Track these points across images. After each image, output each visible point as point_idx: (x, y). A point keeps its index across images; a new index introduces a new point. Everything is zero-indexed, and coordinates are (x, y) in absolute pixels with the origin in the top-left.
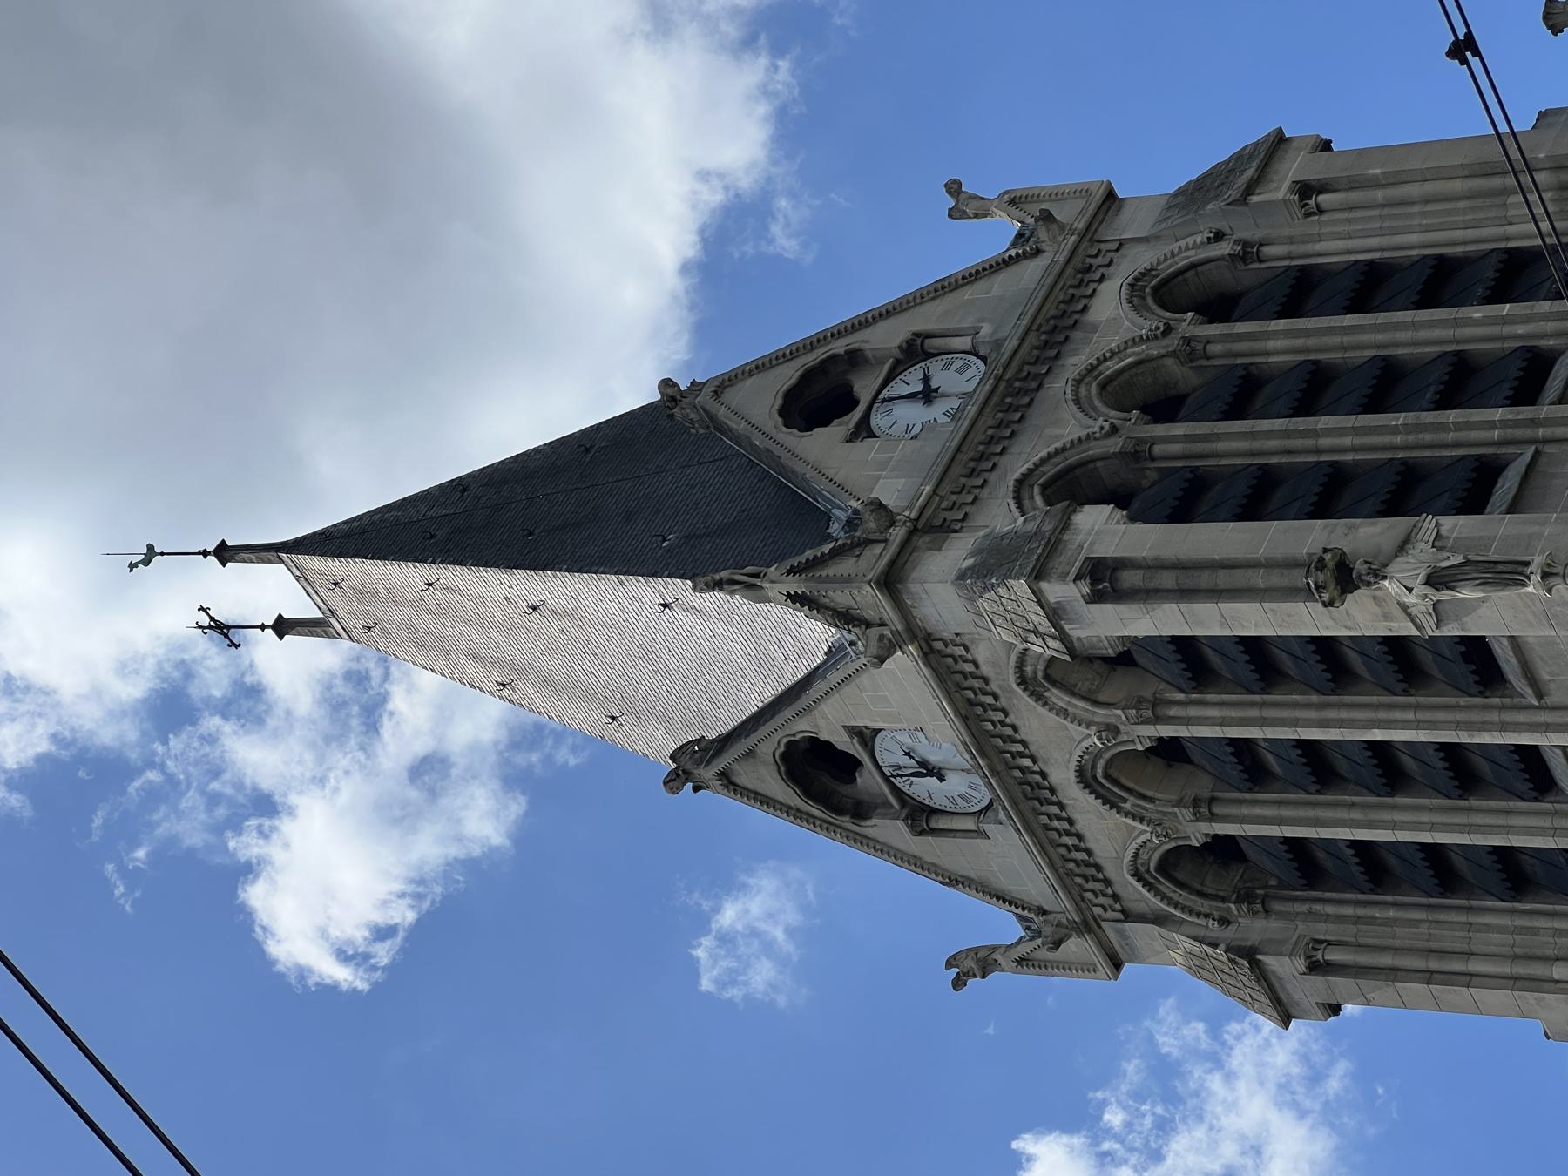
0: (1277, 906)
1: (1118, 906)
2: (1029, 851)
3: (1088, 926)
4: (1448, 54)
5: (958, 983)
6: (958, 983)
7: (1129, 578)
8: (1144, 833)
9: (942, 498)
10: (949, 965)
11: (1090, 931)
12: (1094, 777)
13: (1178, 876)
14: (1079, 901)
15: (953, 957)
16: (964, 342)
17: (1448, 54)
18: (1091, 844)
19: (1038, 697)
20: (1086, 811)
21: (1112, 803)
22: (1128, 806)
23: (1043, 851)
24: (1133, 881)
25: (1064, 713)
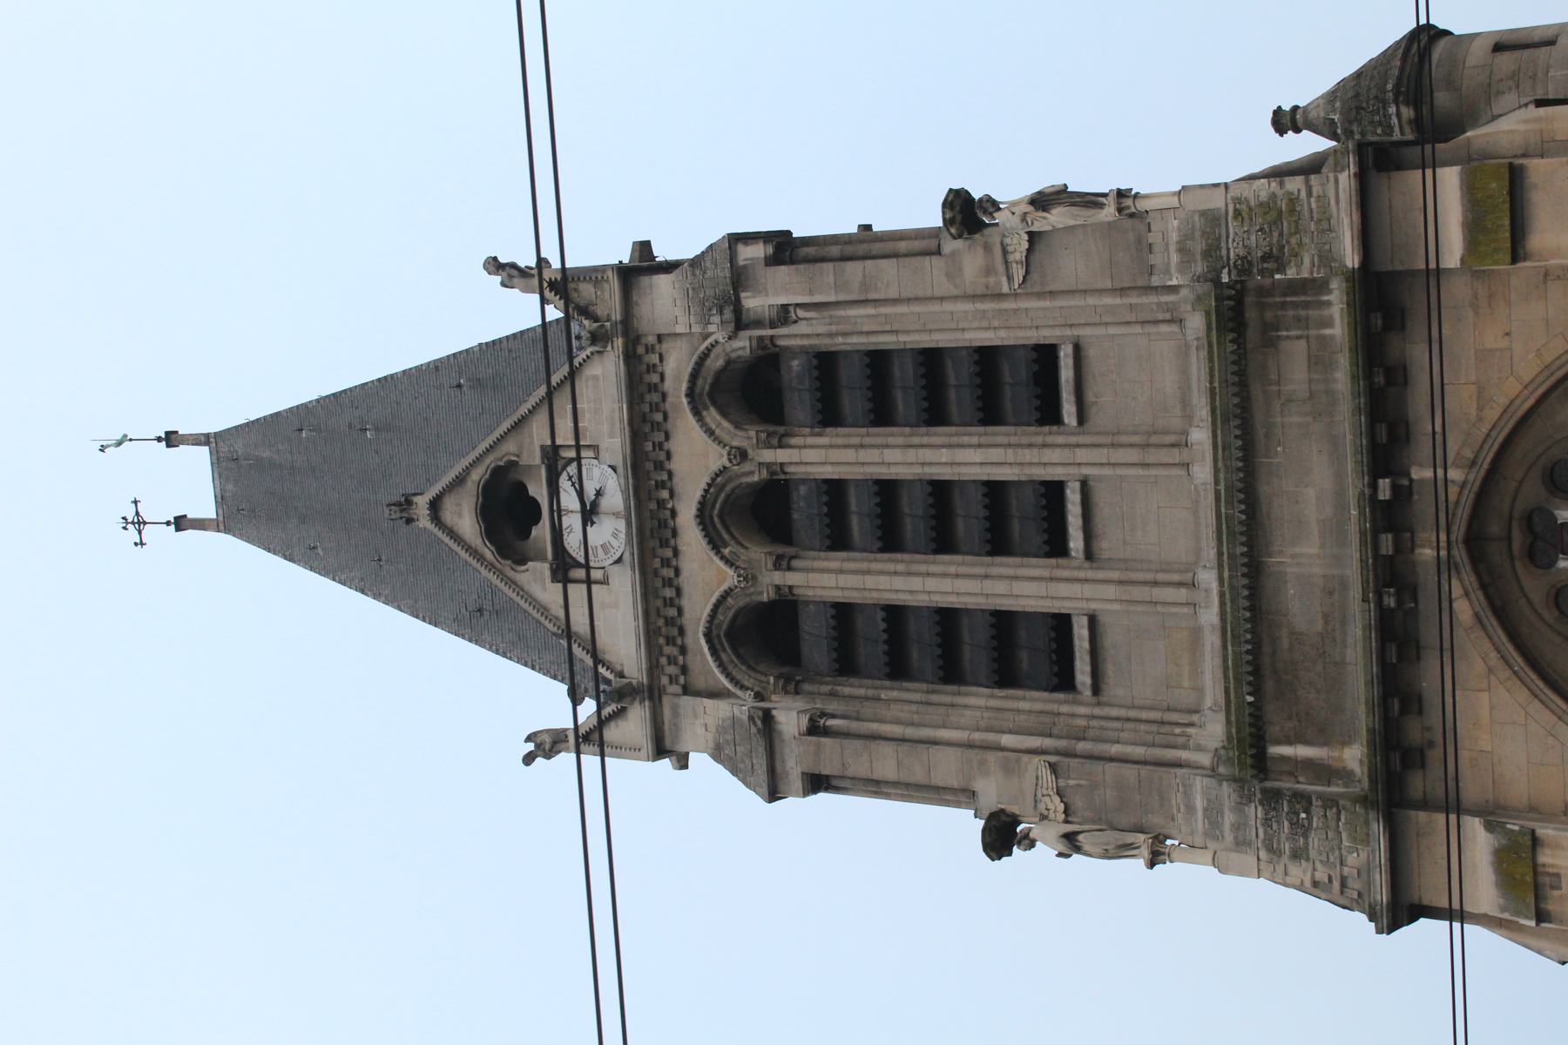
0: (806, 687)
1: (682, 680)
2: (634, 596)
3: (652, 693)
4: (648, 243)
5: (528, 759)
6: (528, 759)
7: (1387, 543)
8: (730, 577)
9: (578, 338)
10: (529, 739)
11: (651, 698)
12: (711, 517)
13: (742, 651)
14: (653, 668)
15: (535, 734)
16: (565, 436)
17: (648, 243)
18: (685, 602)
19: (697, 413)
20: (691, 538)
21: (715, 544)
22: (726, 551)
23: (645, 595)
24: (703, 641)
25: (710, 433)
